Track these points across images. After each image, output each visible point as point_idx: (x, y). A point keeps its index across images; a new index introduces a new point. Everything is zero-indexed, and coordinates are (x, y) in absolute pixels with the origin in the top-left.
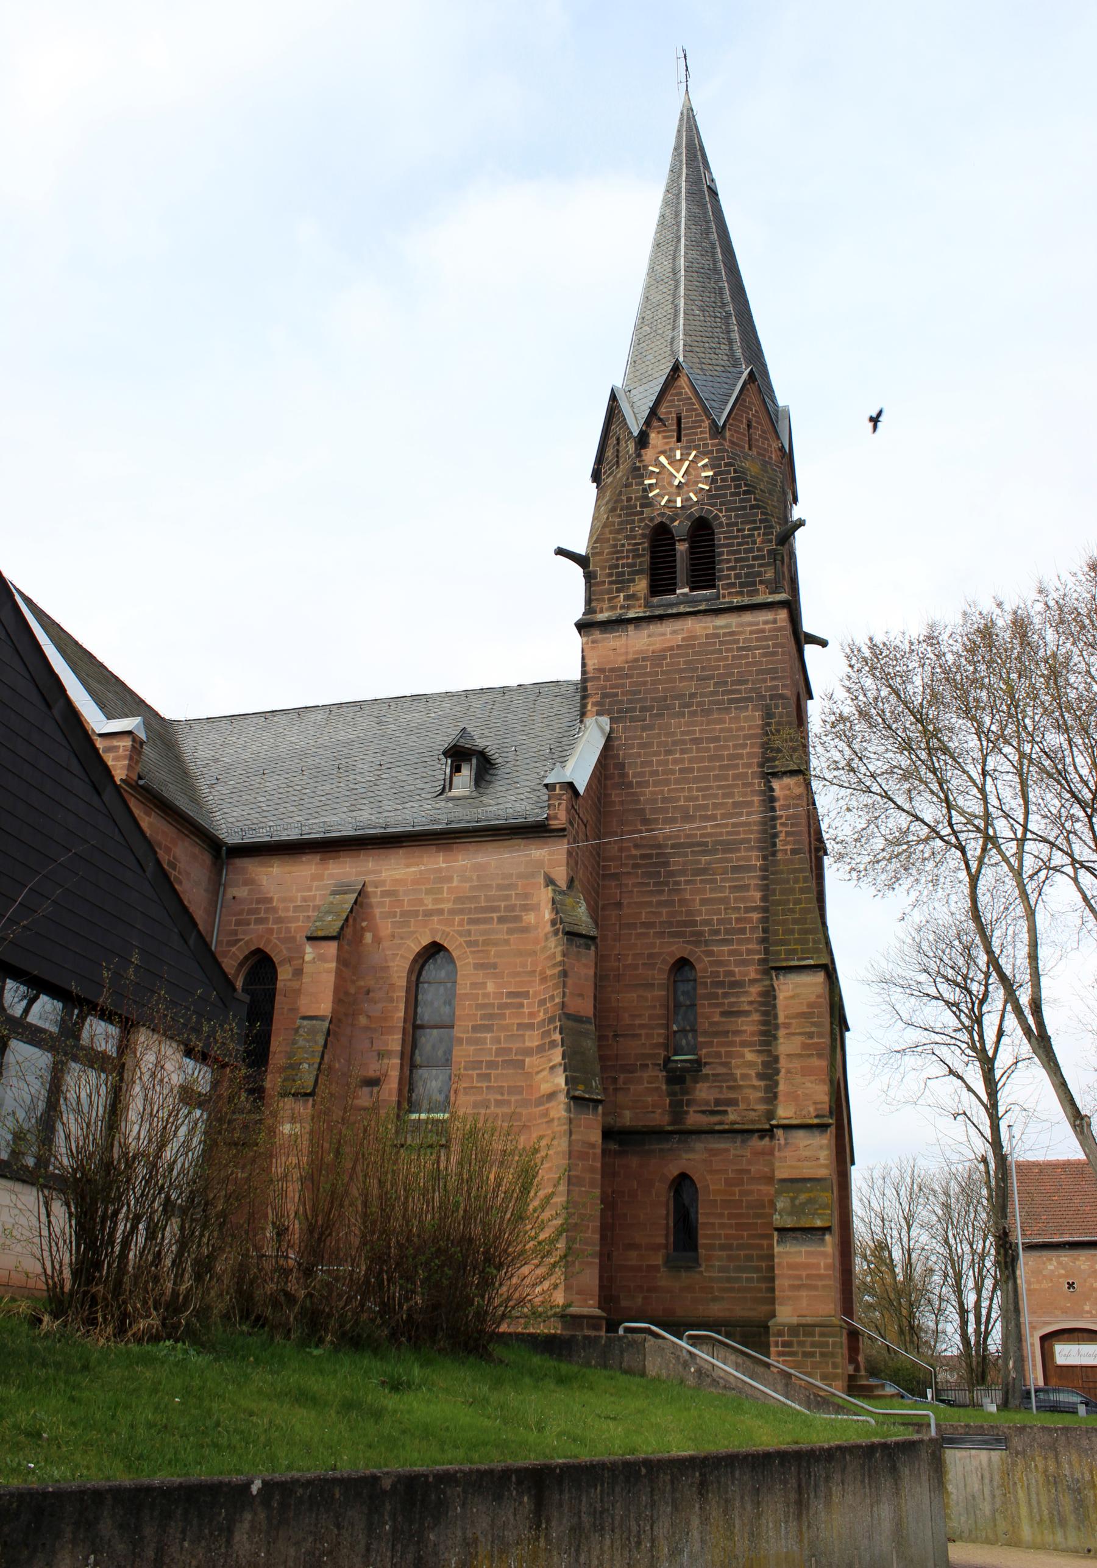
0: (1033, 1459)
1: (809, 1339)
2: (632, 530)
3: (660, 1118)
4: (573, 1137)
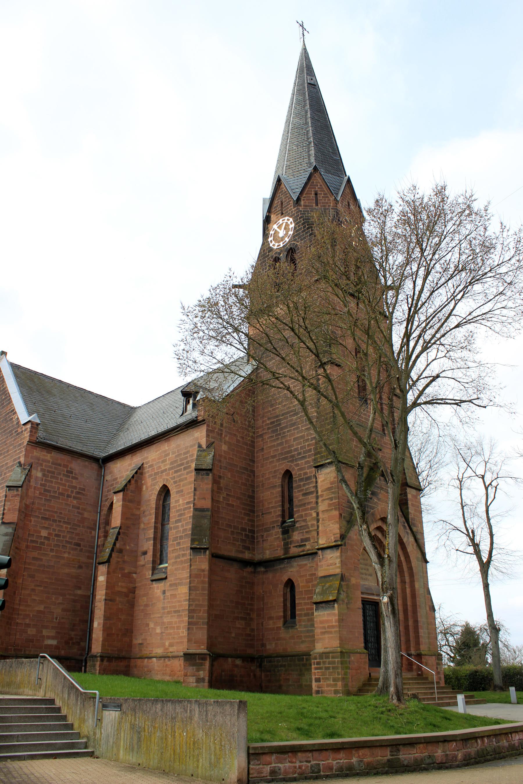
0: (128, 716)
1: (327, 660)
3: (280, 553)
4: (192, 567)
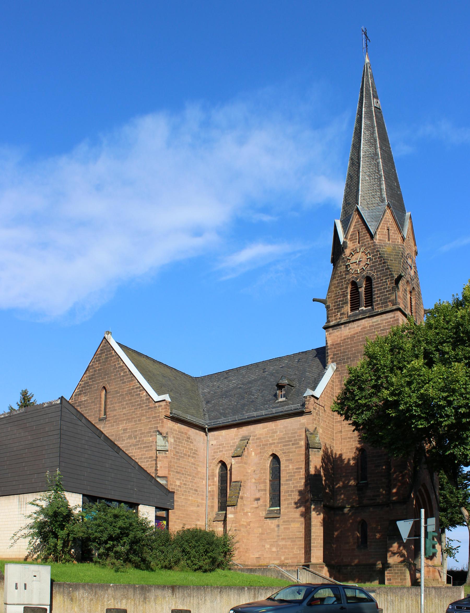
2: (342, 285)
